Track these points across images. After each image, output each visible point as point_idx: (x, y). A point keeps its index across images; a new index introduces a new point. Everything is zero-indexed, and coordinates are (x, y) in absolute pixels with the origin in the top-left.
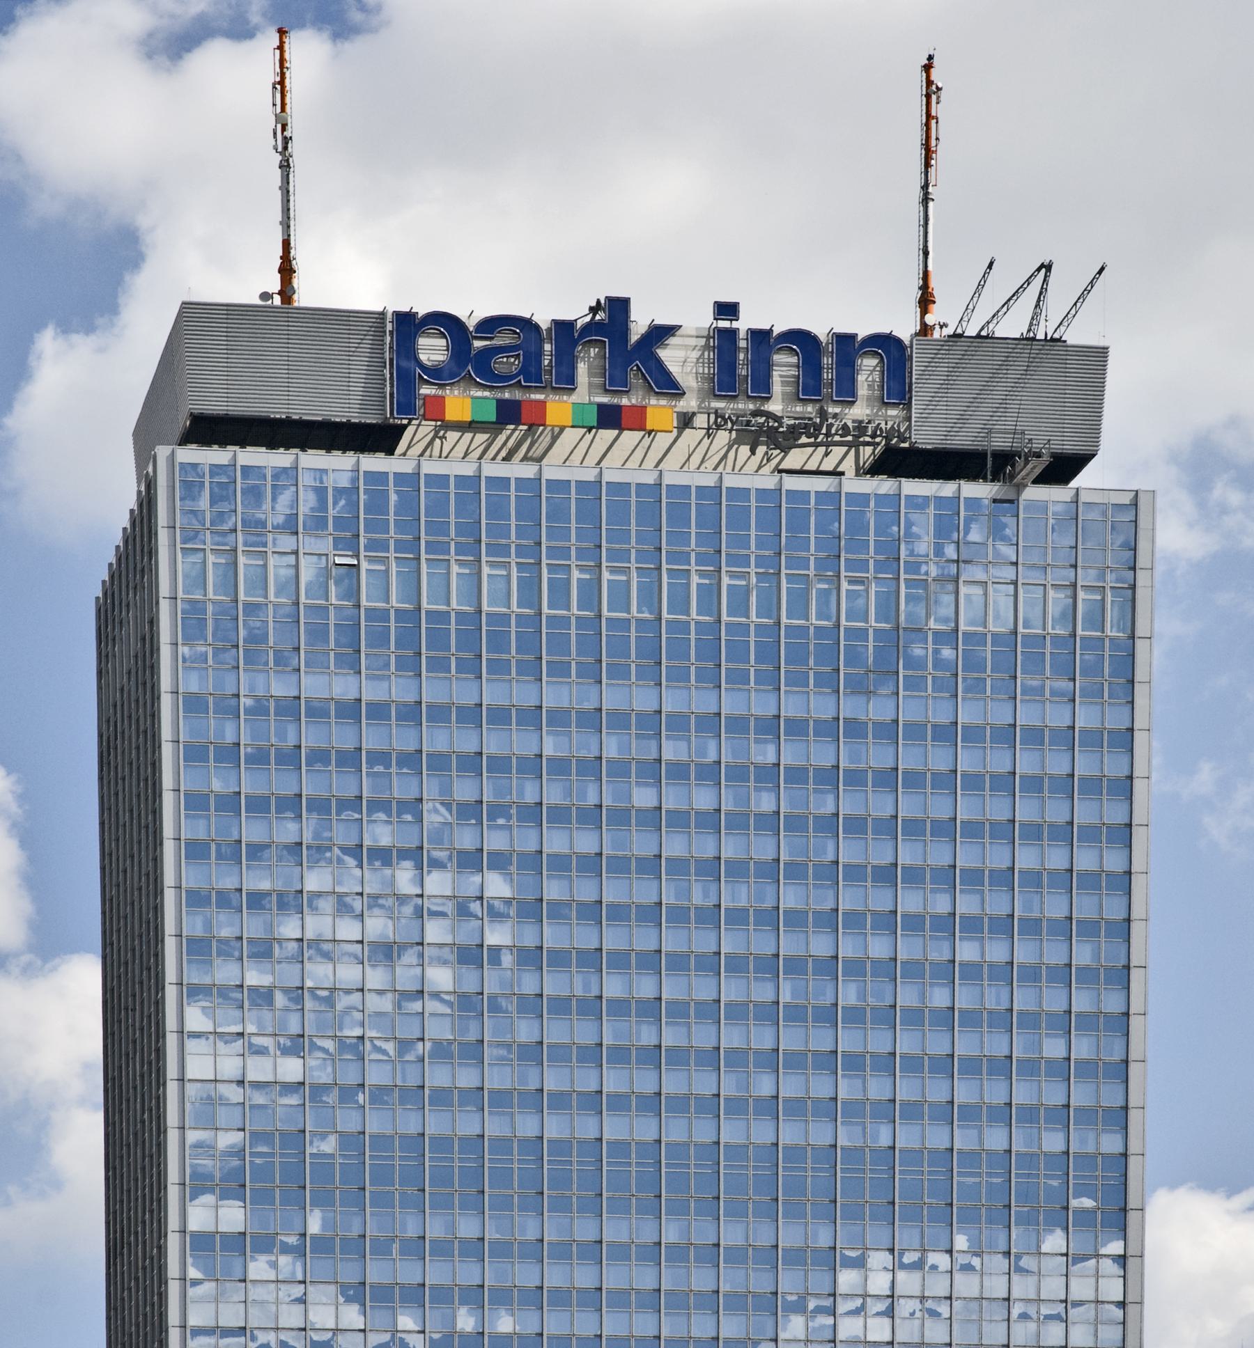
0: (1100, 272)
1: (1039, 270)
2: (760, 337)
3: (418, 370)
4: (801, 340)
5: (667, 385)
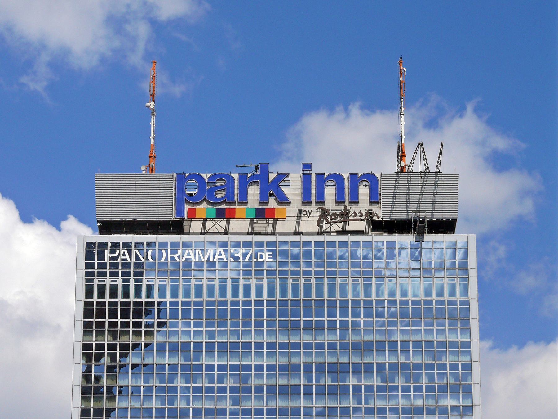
0: (442, 145)
1: (418, 145)
2: (321, 178)
3: (185, 198)
4: (337, 178)
5: (283, 200)
